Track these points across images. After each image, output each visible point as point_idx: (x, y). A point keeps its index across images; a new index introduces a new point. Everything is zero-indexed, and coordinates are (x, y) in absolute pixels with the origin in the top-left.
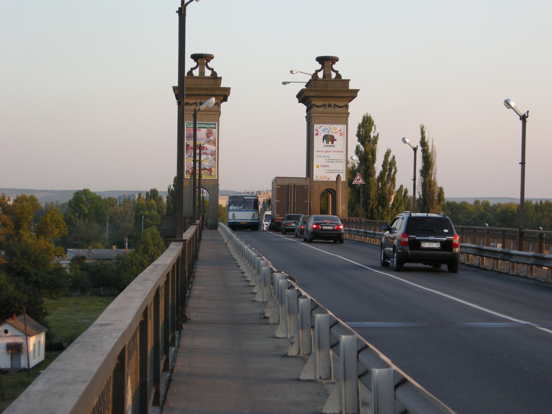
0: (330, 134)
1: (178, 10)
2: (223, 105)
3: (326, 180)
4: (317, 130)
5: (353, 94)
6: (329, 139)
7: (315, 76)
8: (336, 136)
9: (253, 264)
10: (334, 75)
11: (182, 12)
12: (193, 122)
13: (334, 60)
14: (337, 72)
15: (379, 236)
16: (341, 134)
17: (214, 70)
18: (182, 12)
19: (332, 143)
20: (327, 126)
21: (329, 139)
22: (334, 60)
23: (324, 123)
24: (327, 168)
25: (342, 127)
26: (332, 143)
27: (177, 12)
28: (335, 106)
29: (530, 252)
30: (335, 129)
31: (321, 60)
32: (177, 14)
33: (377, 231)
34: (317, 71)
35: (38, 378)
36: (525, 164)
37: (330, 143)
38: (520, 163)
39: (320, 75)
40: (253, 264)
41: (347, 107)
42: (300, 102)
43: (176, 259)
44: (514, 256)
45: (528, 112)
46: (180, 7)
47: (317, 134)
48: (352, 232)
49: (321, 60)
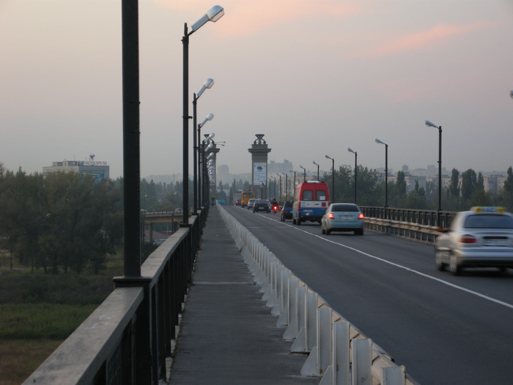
0: (260, 166)
1: (182, 39)
2: (217, 154)
3: (258, 185)
4: (255, 165)
5: (270, 150)
6: (260, 168)
7: (255, 142)
8: (263, 167)
9: (265, 269)
10: (262, 142)
11: (185, 41)
12: (210, 185)
13: (263, 135)
14: (264, 140)
15: (404, 226)
16: (265, 166)
17: (213, 140)
18: (185, 41)
19: (261, 170)
20: (259, 163)
21: (260, 168)
22: (263, 135)
23: (258, 162)
24: (259, 180)
25: (265, 164)
26: (261, 170)
27: (182, 40)
28: (262, 155)
29: (405, 222)
30: (262, 164)
31: (257, 135)
32: (182, 42)
33: (241, 203)
34: (256, 140)
35: (52, 359)
36: (442, 163)
37: (260, 170)
38: (438, 162)
39: (257, 142)
40: (265, 269)
41: (267, 155)
42: (249, 152)
43: (163, 267)
44: (412, 227)
45: (378, 141)
46: (184, 35)
47: (255, 166)
48: (366, 220)
49: (257, 135)
